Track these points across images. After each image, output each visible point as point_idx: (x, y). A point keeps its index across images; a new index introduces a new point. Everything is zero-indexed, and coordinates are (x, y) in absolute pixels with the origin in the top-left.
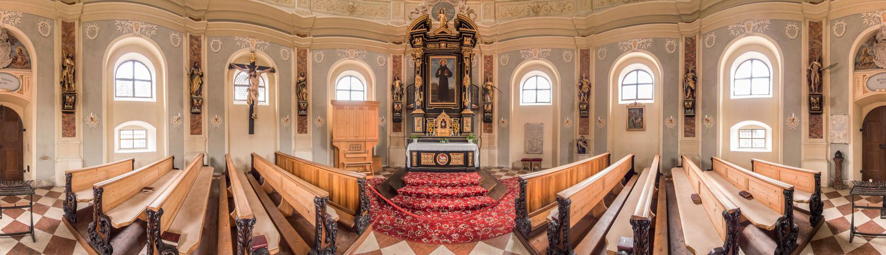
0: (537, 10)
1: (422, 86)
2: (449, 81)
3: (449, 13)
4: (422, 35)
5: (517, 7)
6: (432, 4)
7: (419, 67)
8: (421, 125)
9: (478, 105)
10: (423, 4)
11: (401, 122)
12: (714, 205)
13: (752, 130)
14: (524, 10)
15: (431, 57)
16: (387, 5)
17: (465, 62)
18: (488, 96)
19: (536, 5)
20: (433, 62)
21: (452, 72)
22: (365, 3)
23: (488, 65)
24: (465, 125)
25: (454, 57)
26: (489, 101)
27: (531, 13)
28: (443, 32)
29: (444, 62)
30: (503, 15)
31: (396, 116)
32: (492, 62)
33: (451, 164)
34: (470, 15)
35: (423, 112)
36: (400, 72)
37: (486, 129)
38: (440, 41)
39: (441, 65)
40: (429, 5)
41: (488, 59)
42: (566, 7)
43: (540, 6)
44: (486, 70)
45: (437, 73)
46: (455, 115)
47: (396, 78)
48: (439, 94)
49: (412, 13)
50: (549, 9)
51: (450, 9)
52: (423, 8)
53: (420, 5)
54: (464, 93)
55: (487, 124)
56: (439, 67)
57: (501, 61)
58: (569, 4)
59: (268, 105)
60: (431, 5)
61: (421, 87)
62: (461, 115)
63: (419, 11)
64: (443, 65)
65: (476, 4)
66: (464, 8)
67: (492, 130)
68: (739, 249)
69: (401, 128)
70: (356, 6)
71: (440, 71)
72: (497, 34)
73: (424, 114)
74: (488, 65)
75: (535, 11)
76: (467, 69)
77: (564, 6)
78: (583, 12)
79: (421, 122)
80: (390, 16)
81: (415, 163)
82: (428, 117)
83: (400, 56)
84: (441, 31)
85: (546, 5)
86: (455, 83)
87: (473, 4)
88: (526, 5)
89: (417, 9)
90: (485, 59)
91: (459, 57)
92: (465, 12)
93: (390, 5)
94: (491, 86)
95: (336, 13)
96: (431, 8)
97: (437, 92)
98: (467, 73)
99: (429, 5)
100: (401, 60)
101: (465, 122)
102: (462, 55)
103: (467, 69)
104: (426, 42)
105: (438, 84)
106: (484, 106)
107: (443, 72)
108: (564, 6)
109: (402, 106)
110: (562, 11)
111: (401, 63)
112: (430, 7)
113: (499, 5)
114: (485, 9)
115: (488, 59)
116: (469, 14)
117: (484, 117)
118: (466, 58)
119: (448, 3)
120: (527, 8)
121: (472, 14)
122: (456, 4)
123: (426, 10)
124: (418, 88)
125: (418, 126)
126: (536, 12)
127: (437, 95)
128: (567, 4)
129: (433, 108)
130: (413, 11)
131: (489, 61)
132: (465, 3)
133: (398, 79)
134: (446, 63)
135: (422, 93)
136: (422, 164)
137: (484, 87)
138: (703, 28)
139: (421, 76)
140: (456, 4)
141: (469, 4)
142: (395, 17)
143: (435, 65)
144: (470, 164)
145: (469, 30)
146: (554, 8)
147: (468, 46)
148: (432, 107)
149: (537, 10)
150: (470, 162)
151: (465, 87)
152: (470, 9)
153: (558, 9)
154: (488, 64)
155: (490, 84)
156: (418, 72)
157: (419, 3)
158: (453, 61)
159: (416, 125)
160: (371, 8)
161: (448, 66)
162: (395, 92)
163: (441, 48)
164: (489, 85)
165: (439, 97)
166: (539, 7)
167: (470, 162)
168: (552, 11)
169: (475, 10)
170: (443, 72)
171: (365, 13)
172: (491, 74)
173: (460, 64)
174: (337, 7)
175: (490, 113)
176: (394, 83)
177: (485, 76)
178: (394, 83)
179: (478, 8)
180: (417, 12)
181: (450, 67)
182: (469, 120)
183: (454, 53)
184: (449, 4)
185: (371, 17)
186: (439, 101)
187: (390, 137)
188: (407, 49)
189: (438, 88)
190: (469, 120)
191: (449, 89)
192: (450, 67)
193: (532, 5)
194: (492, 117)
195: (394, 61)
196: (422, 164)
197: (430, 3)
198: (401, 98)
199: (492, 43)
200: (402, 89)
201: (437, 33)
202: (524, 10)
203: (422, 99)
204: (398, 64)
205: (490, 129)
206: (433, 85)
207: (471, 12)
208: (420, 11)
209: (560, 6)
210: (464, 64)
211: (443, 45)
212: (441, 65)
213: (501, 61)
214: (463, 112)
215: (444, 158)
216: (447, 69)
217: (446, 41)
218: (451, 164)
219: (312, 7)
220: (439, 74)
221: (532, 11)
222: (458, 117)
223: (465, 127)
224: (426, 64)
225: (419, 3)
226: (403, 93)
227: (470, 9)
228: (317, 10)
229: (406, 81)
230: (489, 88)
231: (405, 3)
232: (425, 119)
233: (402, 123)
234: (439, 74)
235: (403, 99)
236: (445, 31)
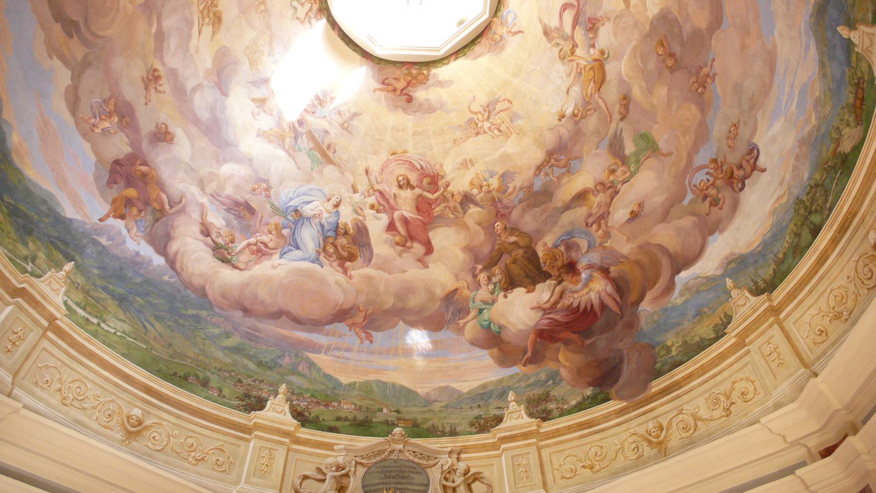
0: (658, 437)
3: (411, 484)
5: (601, 447)
6: (364, 461)
10: (341, 460)
12: (144, 103)
14: (622, 449)
16: (238, 446)
19: (651, 425)
22: (175, 424)
27: (647, 450)
30: (569, 475)
34: (473, 485)
40: (357, 463)
42: (735, 396)
43: (665, 425)
49: (306, 477)
50: (692, 422)
51: (414, 476)
52: (339, 468)
53: (330, 460)
58: (740, 386)
60: (360, 463)
63: (325, 475)
65: (489, 457)
66: (455, 471)
68: (764, 294)
70: (148, 422)
75: (654, 440)
77: (728, 397)
78: (785, 388)
80: (239, 476)
85: (681, 416)
87: (480, 458)
88: (625, 436)
89: (319, 470)
92: (459, 480)
93: (247, 447)
95: (87, 421)
96: (361, 471)
99: (357, 463)
108: (728, 397)
110: (728, 411)
112: (359, 467)
113: (550, 454)
114: (515, 466)
116: (469, 486)
119: (409, 460)
120: (630, 440)
121: (477, 483)
122: (431, 462)
123: (347, 475)
126: (660, 443)
128: (732, 389)
130: (308, 473)
132: (458, 459)
138: (586, 61)
140: (431, 462)
141: (467, 459)
142: (254, 480)
146: (703, 413)
149: (658, 437)
152: (472, 471)
153: (715, 412)
157: (327, 456)
160: (190, 441)
166: (661, 428)
168: (699, 423)
169: (486, 473)
171: (168, 449)
174: (94, 408)
179: (495, 468)
180: (320, 477)
184: (413, 462)
185: (185, 464)
193: (641, 430)
197: (358, 459)
202: (622, 449)
207: (475, 480)
208: (329, 474)
209: (716, 402)
219: (22, 373)
221: (645, 444)
225: (327, 456)
227: (472, 471)
228: (33, 387)
231: (288, 450)
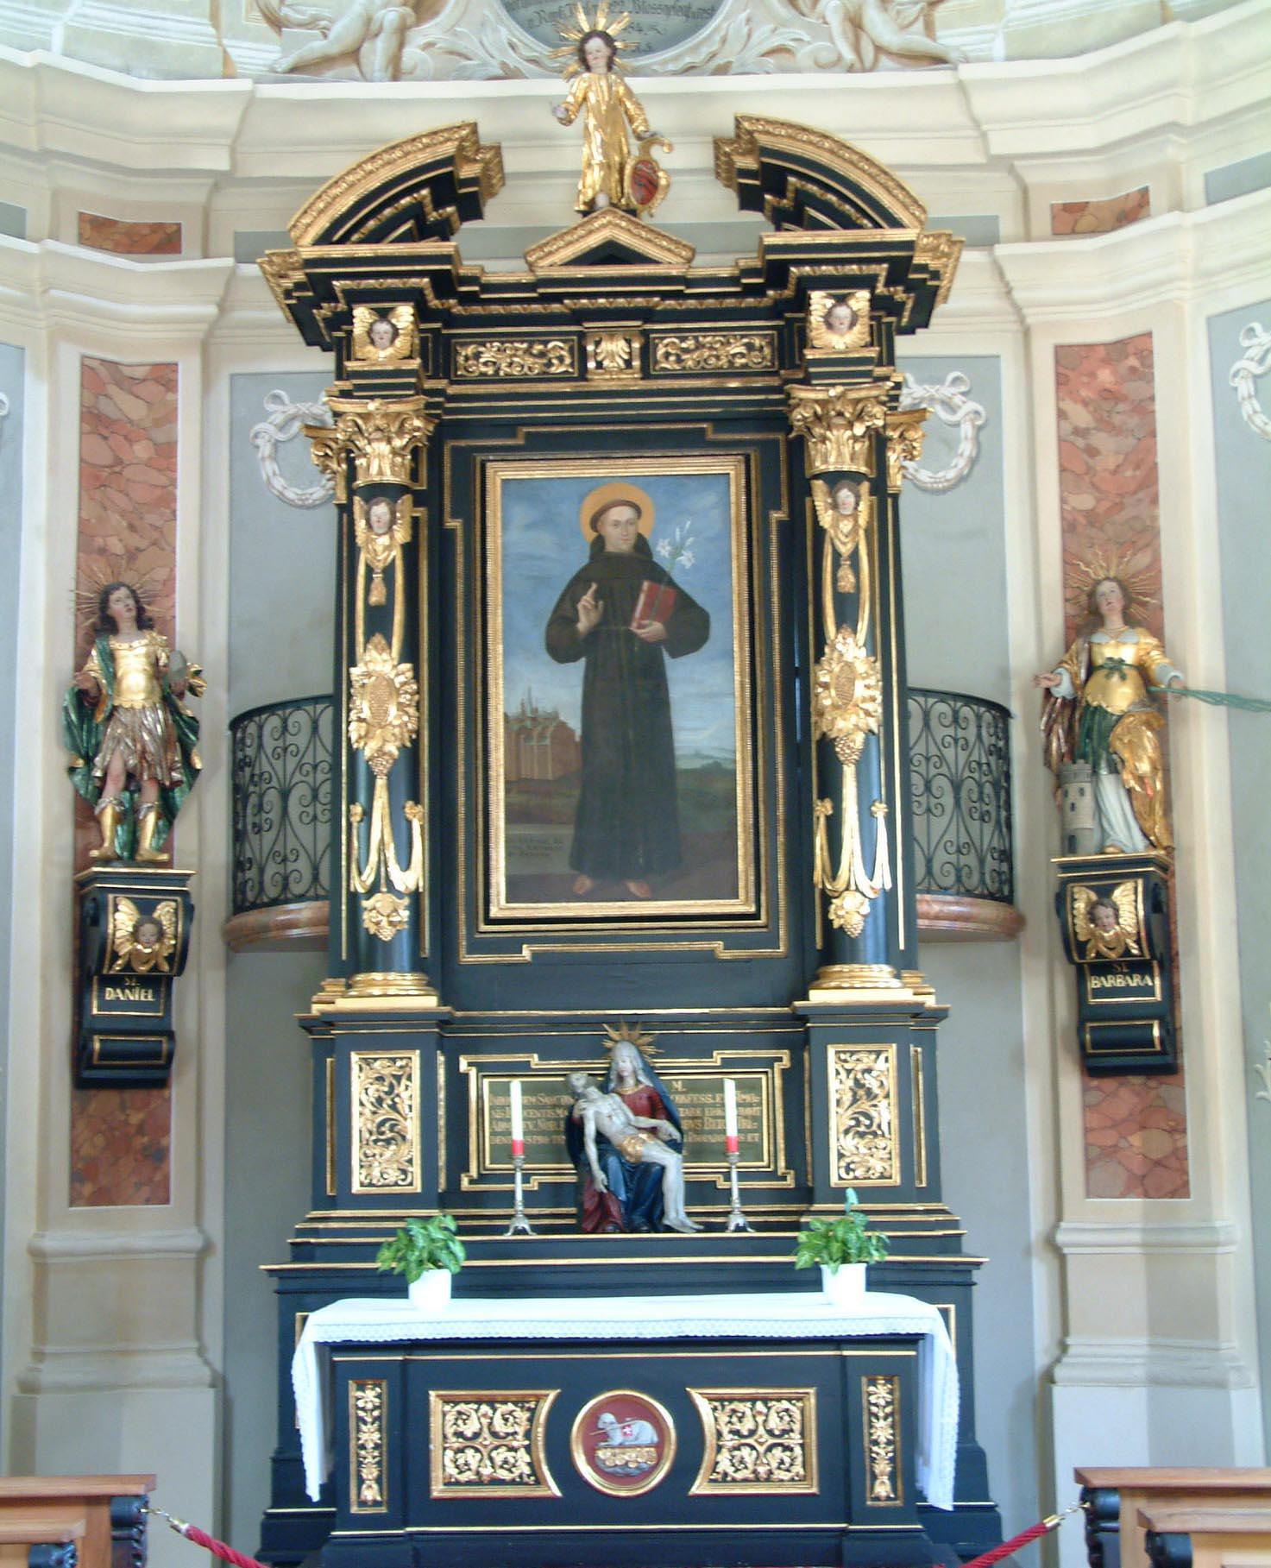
1: (416, 743)
2: (676, 692)
4: (414, 282)
7: (389, 572)
8: (412, 1128)
9: (1008, 899)
11: (162, 1083)
13: (428, 1218)
15: (499, 474)
17: (826, 519)
18: (1108, 784)
20: (521, 514)
21: (700, 599)
23: (1100, 440)
24: (838, 1119)
25: (728, 467)
26: (1127, 838)
28: (611, 253)
29: (623, 513)
31: (110, 1029)
32: (1144, 409)
33: (700, 1487)
35: (430, 1002)
36: (163, 542)
37: (1111, 1152)
38: (578, 317)
39: (599, 543)
41: (1105, 376)
44: (1085, 501)
45: (563, 618)
46: (740, 1021)
47: (121, 605)
48: (581, 819)
54: (823, 809)
55: (1125, 1095)
56: (580, 558)
57: (1245, 387)
59: (419, 1190)
61: (411, 753)
62: (801, 1018)
64: (618, 542)
67: (1180, 1155)
69: (159, 1155)
71: (587, 599)
72: (1174, 127)
73: (444, 1023)
74: (1100, 440)
76: (847, 581)
79: (410, 1094)
81: (371, 1493)
82: (472, 1047)
83: (164, 375)
84: (594, 241)
86: (736, 704)
90: (1061, 381)
91: (768, 448)
94: (1142, 670)
97: (566, 802)
98: (847, 618)
100: (170, 417)
101: (838, 1086)
102: (798, 449)
103: (847, 581)
104: (450, 320)
105: (575, 723)
106: (1061, 901)
107: (616, 608)
109: (189, 911)
111: (166, 453)
115: (1105, 376)
117: (1084, 1013)
118: (835, 479)
124: (382, 767)
125: (387, 1134)
127: (567, 832)
129: (526, 953)
131: (1109, 395)
133: (143, 622)
134: (644, 528)
135: (417, 817)
136: (438, 1490)
137: (1064, 689)
139: (410, 653)
143: (544, 543)
144: (883, 1488)
145: (839, 236)
147: (844, 368)
148: (514, 945)
150: (883, 1467)
151: (827, 745)
154: (1105, 424)
155: (1128, 654)
156: (379, 620)
158: (710, 498)
159: (360, 1122)
161: (662, 551)
162: (114, 759)
163: (599, 382)
164: (1116, 666)
165: (579, 842)
167: (883, 1467)
170: (616, 608)
172: (1145, 535)
173: (776, 516)
175: (1140, 967)
176: (94, 663)
177: (1069, 561)
178: (94, 663)
181: (686, 559)
182: (882, 1066)
183: (720, 422)
186: (586, 883)
187: (39, 1259)
188: (239, 315)
189: (573, 756)
190: (882, 1066)
191: (682, 764)
192: (686, 559)
194: (1168, 1012)
195: (94, 421)
196: (438, 1490)
198: (168, 812)
199: (1132, 210)
200: (183, 733)
201: (554, 263)
203: (412, 877)
204: (141, 450)
205: (1159, 1145)
206: (522, 728)
210: (819, 532)
211: (613, 350)
212: (599, 543)
213: (1245, 387)
214: (817, 997)
215: (643, 1431)
216: (658, 575)
217: (647, 315)
218: (700, 1487)
220: (583, 625)
222: (779, 1043)
223: (840, 1141)
224: (454, 524)
226: (193, 773)
229: (218, 637)
230: (1121, 697)
232: (452, 1066)
233: (180, 1092)
234: (583, 625)
235: (184, 829)
236: (625, 239)
